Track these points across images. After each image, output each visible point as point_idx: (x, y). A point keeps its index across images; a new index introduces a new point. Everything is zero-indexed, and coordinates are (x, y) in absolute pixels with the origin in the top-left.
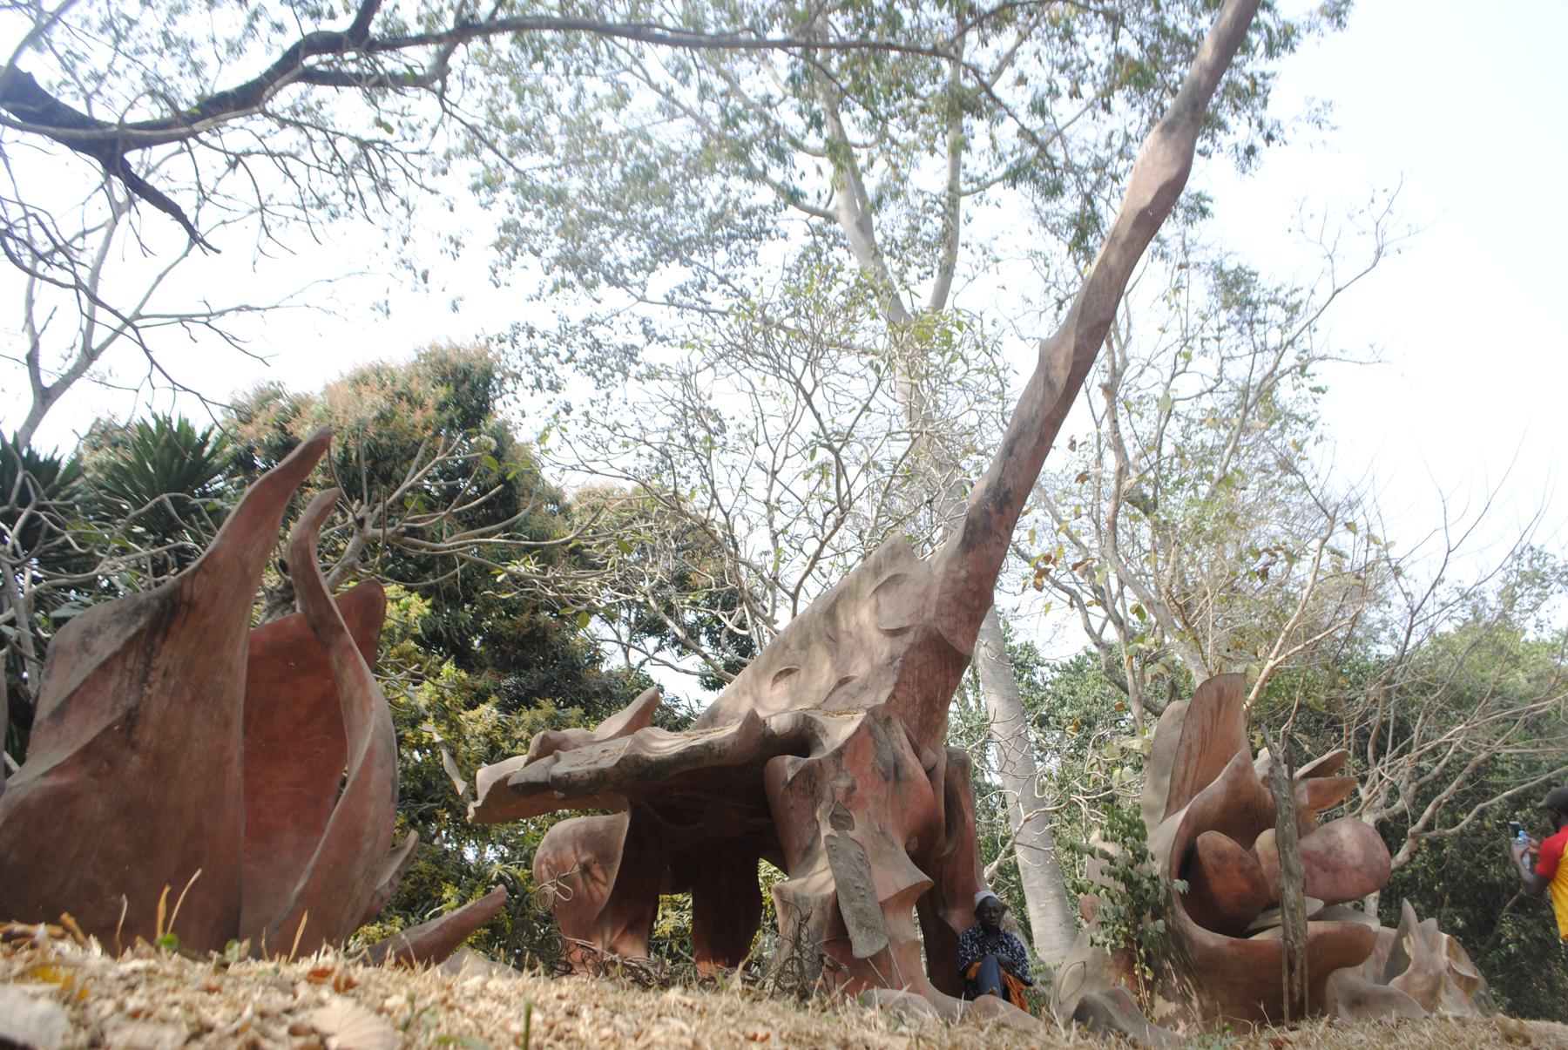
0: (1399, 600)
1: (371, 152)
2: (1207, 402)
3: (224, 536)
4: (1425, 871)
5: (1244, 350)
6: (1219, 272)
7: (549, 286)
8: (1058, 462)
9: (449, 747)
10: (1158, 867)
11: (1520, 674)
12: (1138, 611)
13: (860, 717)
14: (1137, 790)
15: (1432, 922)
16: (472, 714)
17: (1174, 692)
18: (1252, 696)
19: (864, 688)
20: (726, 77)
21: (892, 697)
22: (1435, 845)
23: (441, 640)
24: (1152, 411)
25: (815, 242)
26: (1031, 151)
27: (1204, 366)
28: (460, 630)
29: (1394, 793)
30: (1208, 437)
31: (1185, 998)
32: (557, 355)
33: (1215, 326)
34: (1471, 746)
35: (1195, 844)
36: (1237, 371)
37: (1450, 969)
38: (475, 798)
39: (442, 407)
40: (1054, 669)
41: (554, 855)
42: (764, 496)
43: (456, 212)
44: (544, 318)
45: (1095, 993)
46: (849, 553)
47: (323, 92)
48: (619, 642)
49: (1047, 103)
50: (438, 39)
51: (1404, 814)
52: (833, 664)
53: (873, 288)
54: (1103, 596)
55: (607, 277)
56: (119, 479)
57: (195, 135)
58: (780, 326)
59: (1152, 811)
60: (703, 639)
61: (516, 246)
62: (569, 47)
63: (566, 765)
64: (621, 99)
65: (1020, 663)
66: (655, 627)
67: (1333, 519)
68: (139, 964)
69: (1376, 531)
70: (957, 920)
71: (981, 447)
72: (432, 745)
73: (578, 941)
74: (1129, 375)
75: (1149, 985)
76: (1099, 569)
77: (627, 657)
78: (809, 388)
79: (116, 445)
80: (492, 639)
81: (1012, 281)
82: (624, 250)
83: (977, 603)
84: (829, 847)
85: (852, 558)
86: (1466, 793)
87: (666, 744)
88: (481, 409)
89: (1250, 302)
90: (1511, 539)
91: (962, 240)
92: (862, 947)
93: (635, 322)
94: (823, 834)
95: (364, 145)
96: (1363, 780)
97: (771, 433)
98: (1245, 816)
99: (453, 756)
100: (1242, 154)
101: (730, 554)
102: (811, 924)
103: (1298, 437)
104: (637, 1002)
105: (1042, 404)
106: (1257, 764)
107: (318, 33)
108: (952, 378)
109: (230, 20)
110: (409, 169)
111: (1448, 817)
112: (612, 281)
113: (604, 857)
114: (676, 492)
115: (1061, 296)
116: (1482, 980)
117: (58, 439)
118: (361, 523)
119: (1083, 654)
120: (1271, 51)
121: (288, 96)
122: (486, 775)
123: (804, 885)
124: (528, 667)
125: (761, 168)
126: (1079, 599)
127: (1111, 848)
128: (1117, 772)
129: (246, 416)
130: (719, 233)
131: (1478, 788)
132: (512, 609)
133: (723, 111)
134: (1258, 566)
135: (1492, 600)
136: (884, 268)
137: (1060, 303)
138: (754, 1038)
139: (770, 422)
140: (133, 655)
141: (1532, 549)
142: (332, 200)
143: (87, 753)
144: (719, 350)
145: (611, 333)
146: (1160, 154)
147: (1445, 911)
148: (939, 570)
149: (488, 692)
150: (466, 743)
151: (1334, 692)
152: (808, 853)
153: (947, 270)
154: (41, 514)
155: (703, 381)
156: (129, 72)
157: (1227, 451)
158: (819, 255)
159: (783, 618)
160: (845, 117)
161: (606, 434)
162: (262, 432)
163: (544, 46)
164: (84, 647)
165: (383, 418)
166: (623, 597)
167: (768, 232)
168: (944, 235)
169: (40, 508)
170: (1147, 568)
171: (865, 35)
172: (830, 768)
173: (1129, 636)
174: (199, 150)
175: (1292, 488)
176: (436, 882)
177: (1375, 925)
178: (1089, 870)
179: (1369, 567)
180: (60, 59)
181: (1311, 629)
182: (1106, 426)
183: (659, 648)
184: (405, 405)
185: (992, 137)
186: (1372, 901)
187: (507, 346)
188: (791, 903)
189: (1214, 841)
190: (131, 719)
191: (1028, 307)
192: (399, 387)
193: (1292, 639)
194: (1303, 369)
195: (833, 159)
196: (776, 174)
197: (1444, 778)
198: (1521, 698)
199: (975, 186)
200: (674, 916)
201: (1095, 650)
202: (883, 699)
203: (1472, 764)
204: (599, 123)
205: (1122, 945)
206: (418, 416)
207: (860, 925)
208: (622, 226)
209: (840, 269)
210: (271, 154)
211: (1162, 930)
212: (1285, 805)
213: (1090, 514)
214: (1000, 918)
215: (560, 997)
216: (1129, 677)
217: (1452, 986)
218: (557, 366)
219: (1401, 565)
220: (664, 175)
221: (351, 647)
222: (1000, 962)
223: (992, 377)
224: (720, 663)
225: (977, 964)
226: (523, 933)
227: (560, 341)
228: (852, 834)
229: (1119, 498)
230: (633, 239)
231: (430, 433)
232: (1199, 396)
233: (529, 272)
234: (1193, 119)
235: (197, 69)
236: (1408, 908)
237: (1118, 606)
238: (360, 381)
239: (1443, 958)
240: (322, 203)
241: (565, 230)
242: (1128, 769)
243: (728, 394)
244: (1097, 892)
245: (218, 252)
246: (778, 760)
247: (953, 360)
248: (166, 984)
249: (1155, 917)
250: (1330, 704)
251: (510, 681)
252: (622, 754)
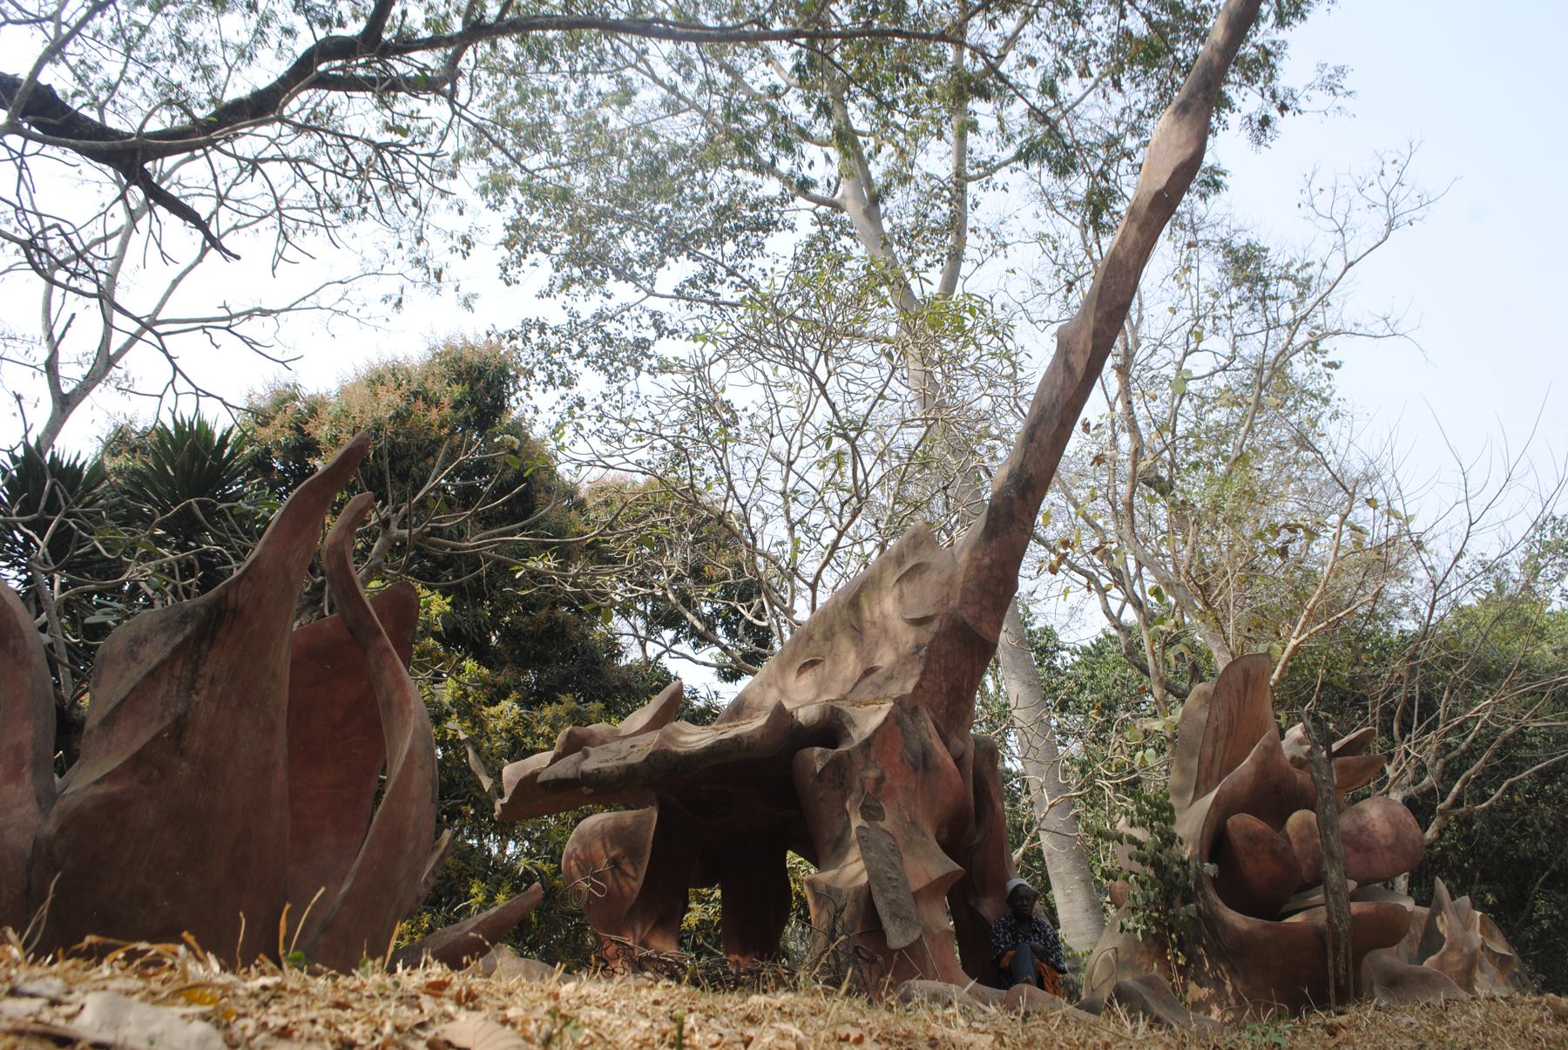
0: (1421, 574)
1: (387, 156)
2: (1220, 381)
3: (267, 543)
4: (1454, 847)
5: (1255, 327)
6: (1227, 248)
7: (559, 282)
8: (1077, 445)
9: (473, 744)
10: (1187, 852)
11: (1545, 646)
12: (1156, 592)
13: (887, 707)
14: (1157, 772)
15: (1465, 900)
16: (493, 710)
17: (1196, 673)
18: (1275, 676)
19: (890, 678)
20: (729, 70)
21: (918, 686)
22: (1466, 821)
23: (457, 637)
24: (1166, 392)
25: (822, 231)
26: (1040, 131)
27: (1218, 344)
28: (479, 627)
29: (1421, 770)
30: (1218, 416)
31: (1219, 983)
32: (569, 350)
33: (1226, 303)
34: (1498, 721)
35: (1225, 826)
36: (1251, 347)
37: (1483, 947)
38: (501, 794)
39: (458, 405)
40: (1074, 652)
41: (583, 850)
42: (779, 486)
43: (469, 212)
44: (554, 313)
45: (1128, 979)
46: (866, 545)
47: (335, 96)
48: (636, 636)
49: (1058, 83)
50: (450, 41)
51: (1432, 791)
52: (858, 654)
53: (886, 277)
54: (1121, 578)
55: (617, 273)
56: (138, 483)
57: (213, 143)
58: (792, 317)
59: (1180, 792)
60: (719, 631)
61: (526, 243)
62: (574, 45)
63: (595, 761)
64: (625, 95)
65: (1043, 646)
66: (673, 620)
67: (1352, 496)
68: (268, 981)
69: (1397, 506)
70: (989, 908)
71: (996, 432)
72: (455, 743)
73: (614, 937)
74: (1140, 355)
75: (1182, 970)
76: (1116, 552)
77: (644, 650)
78: (823, 377)
79: (134, 450)
80: (509, 635)
81: (1021, 260)
82: (630, 245)
83: (1001, 590)
84: (860, 838)
85: (869, 547)
86: (1494, 768)
87: (695, 738)
88: (495, 407)
89: (1261, 279)
90: (1534, 510)
91: (970, 225)
92: (897, 937)
93: (646, 316)
94: (854, 826)
95: (379, 148)
96: (1391, 757)
97: (786, 423)
98: (1275, 795)
99: (477, 751)
100: (1256, 125)
101: (747, 545)
102: (845, 915)
103: (1313, 413)
104: (728, 1005)
105: (1062, 389)
106: (1284, 743)
107: (329, 38)
108: (965, 364)
109: (236, 25)
110: (422, 169)
111: (1477, 792)
112: (619, 274)
113: (633, 853)
114: (692, 486)
115: (1071, 278)
116: (1516, 958)
117: (79, 443)
118: (385, 523)
119: (1101, 636)
120: (1281, 21)
121: (299, 104)
122: (511, 772)
123: (836, 877)
124: (547, 662)
125: (768, 160)
126: (1097, 582)
127: (1140, 834)
128: (1140, 754)
129: (262, 417)
130: (727, 225)
131: (1507, 762)
132: (530, 605)
133: (727, 106)
134: (1277, 544)
135: (1515, 571)
136: (894, 258)
137: (1070, 285)
138: (847, 1038)
139: (784, 412)
140: (180, 662)
141: (1554, 519)
142: (345, 202)
143: (137, 761)
144: (732, 342)
145: (622, 328)
146: (1173, 136)
147: (1475, 888)
148: (963, 558)
149: (509, 688)
150: (489, 740)
151: (1357, 669)
152: (839, 848)
153: (956, 256)
154: (70, 521)
155: (716, 372)
156: (143, 79)
157: (1243, 429)
158: (827, 244)
159: (802, 612)
160: (851, 107)
161: (621, 428)
162: (278, 434)
163: (549, 46)
164: (132, 656)
165: (400, 417)
166: (642, 590)
167: (775, 223)
168: (953, 219)
169: (68, 515)
170: (1164, 550)
171: (869, 23)
173: (1149, 619)
174: (215, 155)
175: (1308, 464)
176: (464, 877)
177: (1409, 904)
178: (1116, 857)
179: (1390, 542)
180: (74, 71)
181: (1333, 606)
182: (1119, 407)
183: (676, 641)
184: (420, 404)
185: (999, 119)
186: (1402, 882)
187: (519, 343)
188: (824, 895)
189: (1244, 823)
190: (180, 726)
191: (1037, 290)
192: (414, 387)
193: (1313, 617)
194: (1315, 344)
195: (841, 147)
196: (784, 165)
197: (1471, 754)
198: (1547, 671)
199: (981, 170)
200: (703, 909)
201: (1113, 632)
202: (910, 687)
203: (1500, 739)
204: (606, 121)
205: (1154, 930)
206: (434, 415)
207: (894, 916)
208: (630, 221)
209: (849, 257)
210: (286, 158)
211: (1194, 914)
212: (1324, 788)
213: (1106, 496)
214: (1032, 905)
215: (656, 1003)
216: (1150, 659)
217: (1487, 964)
218: (569, 362)
219: (1423, 539)
220: (672, 169)
221: (388, 650)
222: (1034, 951)
223: (1006, 362)
224: (738, 654)
225: (1011, 953)
226: (557, 932)
227: (572, 336)
228: (882, 825)
229: (1135, 479)
230: (642, 234)
231: (446, 431)
232: (1212, 374)
233: (539, 270)
234: (1206, 100)
235: (208, 72)
236: (1441, 886)
237: (1137, 588)
238: (376, 380)
239: (1477, 937)
240: (337, 207)
241: (574, 225)
242: (1151, 751)
243: (742, 390)
244: (1126, 879)
245: (238, 258)
246: (806, 751)
247: (965, 345)
248: (296, 1000)
249: (1185, 902)
250: (1353, 681)
251: (531, 677)
252: (651, 748)
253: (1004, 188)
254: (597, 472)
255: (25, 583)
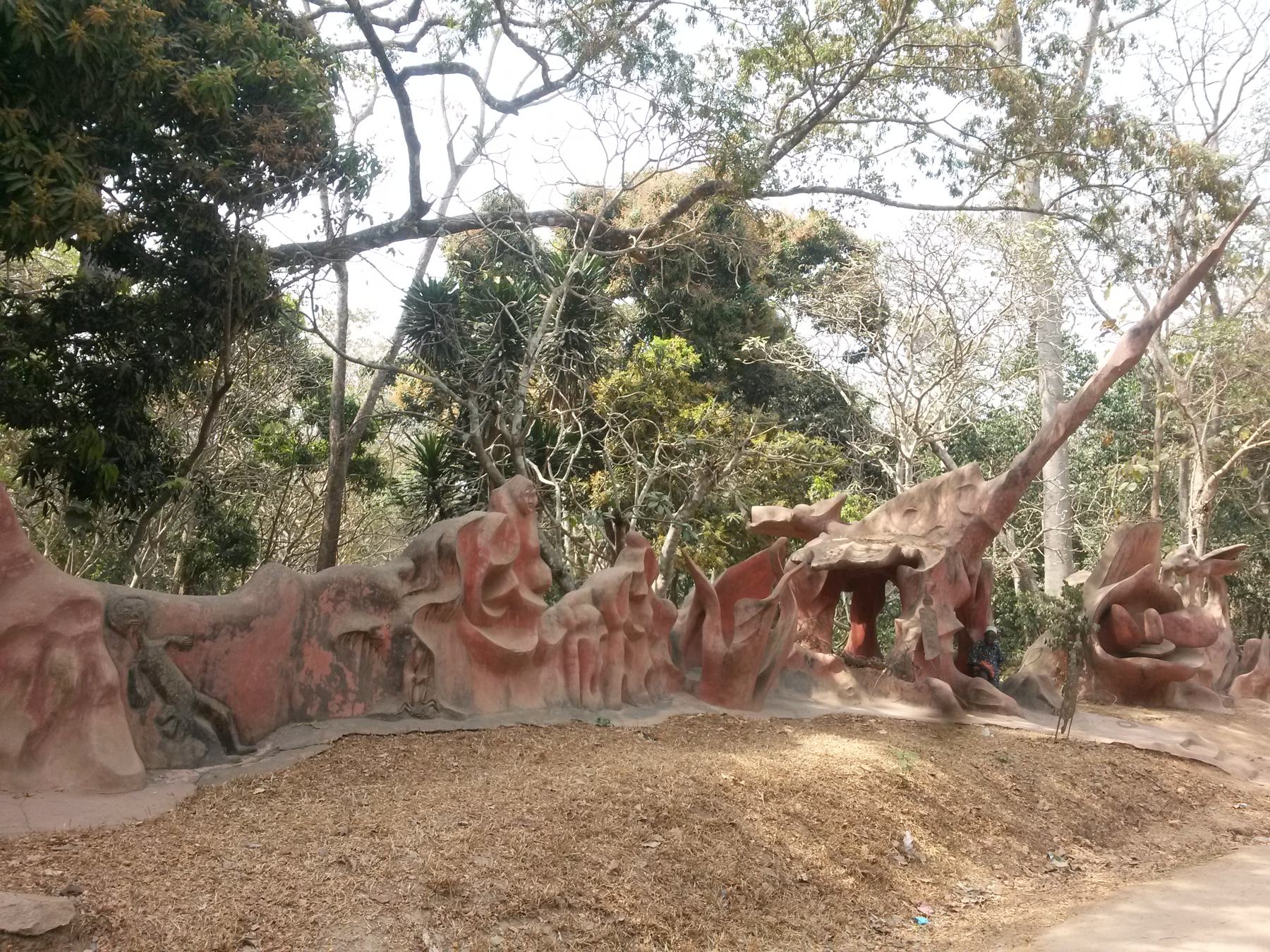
31: (1089, 678)
70: (975, 635)
172: (926, 576)
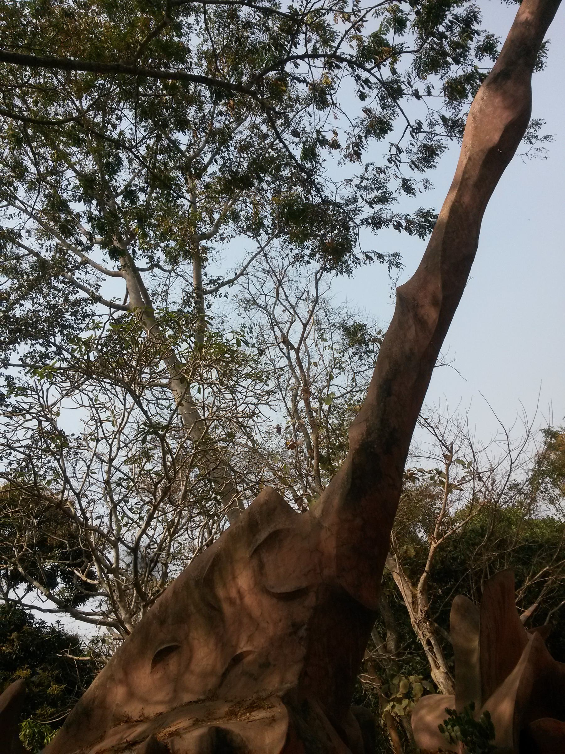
19: (265, 665)
21: (303, 675)
253: (225, 296)
254: (70, 506)
255: (10, 507)
